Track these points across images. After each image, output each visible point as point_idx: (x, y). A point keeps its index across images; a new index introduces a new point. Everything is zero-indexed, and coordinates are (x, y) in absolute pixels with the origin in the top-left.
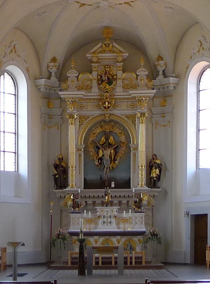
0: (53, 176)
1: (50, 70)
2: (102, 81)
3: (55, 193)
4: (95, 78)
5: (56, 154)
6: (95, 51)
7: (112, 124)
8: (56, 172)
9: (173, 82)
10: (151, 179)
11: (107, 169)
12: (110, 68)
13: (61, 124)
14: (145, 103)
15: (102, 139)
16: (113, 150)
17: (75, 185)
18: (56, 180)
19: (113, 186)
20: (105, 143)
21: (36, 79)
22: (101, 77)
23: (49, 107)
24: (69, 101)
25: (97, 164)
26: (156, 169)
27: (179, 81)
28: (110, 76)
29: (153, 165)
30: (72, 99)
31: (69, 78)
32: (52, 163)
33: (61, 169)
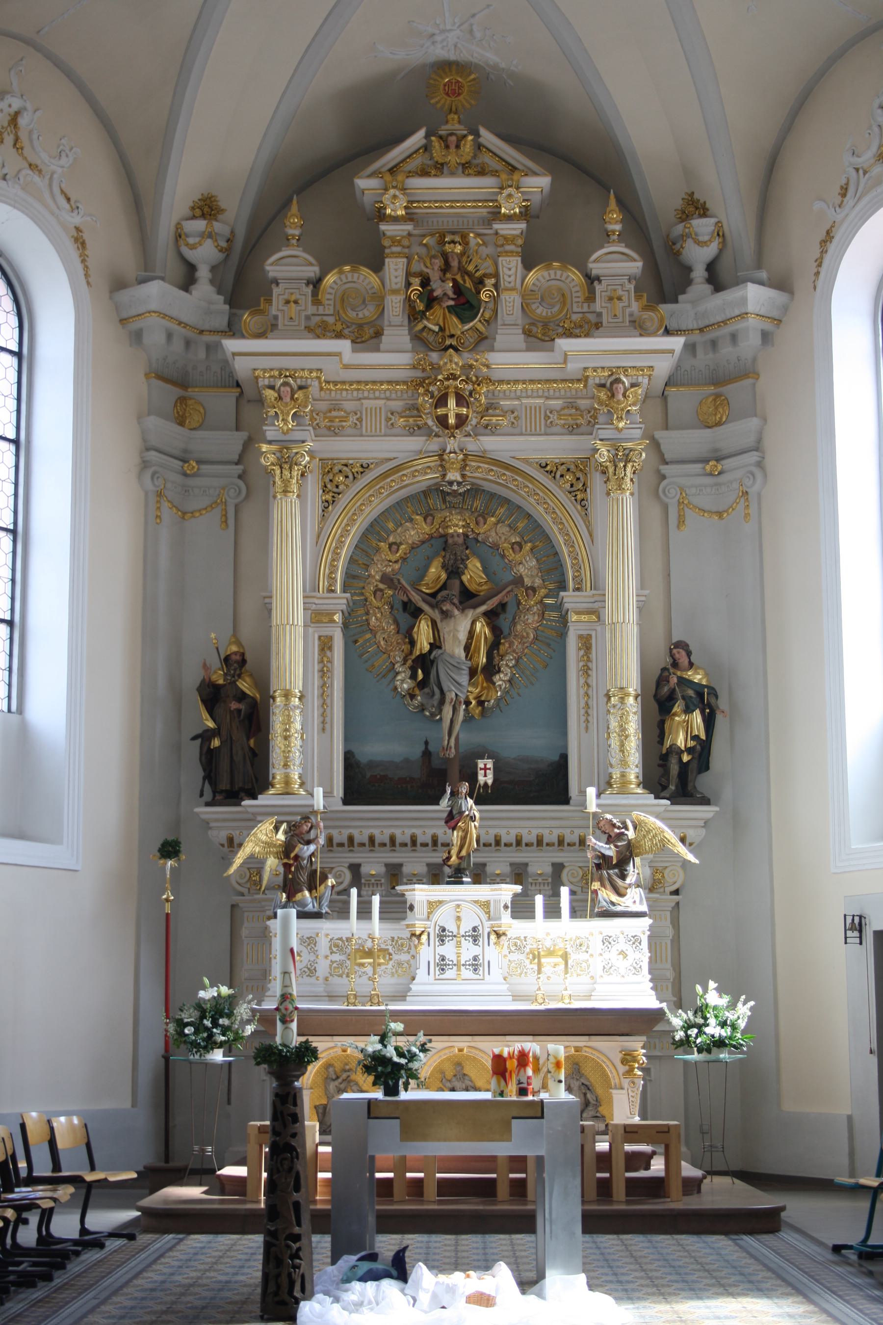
0: (199, 741)
1: (185, 250)
2: (431, 301)
3: (206, 825)
4: (394, 287)
5: (213, 636)
6: (395, 166)
7: (477, 504)
8: (211, 724)
9: (757, 311)
10: (665, 758)
11: (455, 710)
12: (465, 242)
13: (237, 506)
14: (631, 399)
15: (433, 570)
16: (482, 620)
17: (302, 785)
18: (209, 759)
19: (486, 778)
20: (444, 587)
21: (118, 285)
22: (425, 282)
23: (181, 423)
24: (272, 387)
25: (405, 686)
26: (688, 710)
27: (785, 309)
28: (466, 278)
29: (673, 692)
30: (286, 376)
31: (273, 286)
32: (192, 678)
33: (234, 705)
